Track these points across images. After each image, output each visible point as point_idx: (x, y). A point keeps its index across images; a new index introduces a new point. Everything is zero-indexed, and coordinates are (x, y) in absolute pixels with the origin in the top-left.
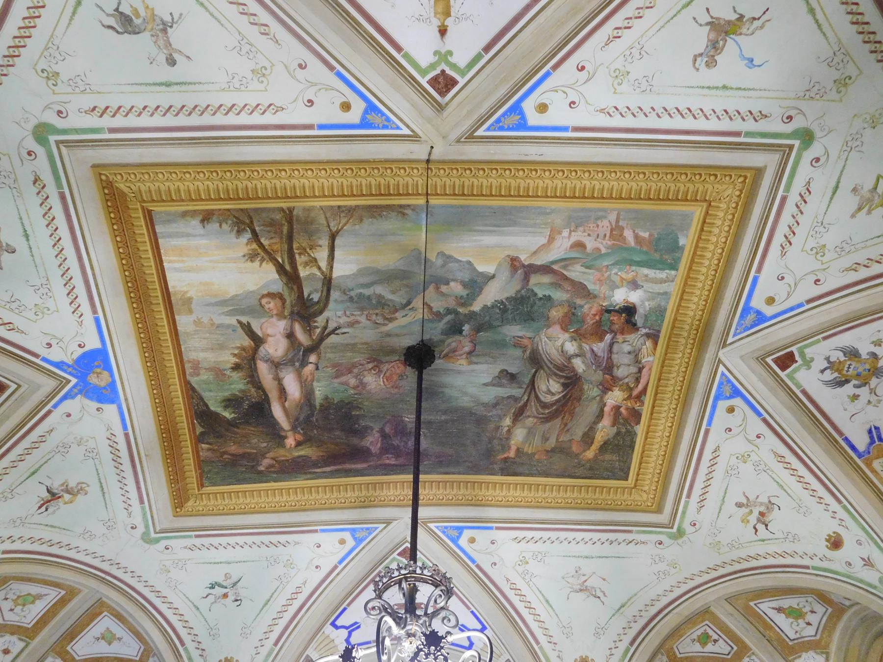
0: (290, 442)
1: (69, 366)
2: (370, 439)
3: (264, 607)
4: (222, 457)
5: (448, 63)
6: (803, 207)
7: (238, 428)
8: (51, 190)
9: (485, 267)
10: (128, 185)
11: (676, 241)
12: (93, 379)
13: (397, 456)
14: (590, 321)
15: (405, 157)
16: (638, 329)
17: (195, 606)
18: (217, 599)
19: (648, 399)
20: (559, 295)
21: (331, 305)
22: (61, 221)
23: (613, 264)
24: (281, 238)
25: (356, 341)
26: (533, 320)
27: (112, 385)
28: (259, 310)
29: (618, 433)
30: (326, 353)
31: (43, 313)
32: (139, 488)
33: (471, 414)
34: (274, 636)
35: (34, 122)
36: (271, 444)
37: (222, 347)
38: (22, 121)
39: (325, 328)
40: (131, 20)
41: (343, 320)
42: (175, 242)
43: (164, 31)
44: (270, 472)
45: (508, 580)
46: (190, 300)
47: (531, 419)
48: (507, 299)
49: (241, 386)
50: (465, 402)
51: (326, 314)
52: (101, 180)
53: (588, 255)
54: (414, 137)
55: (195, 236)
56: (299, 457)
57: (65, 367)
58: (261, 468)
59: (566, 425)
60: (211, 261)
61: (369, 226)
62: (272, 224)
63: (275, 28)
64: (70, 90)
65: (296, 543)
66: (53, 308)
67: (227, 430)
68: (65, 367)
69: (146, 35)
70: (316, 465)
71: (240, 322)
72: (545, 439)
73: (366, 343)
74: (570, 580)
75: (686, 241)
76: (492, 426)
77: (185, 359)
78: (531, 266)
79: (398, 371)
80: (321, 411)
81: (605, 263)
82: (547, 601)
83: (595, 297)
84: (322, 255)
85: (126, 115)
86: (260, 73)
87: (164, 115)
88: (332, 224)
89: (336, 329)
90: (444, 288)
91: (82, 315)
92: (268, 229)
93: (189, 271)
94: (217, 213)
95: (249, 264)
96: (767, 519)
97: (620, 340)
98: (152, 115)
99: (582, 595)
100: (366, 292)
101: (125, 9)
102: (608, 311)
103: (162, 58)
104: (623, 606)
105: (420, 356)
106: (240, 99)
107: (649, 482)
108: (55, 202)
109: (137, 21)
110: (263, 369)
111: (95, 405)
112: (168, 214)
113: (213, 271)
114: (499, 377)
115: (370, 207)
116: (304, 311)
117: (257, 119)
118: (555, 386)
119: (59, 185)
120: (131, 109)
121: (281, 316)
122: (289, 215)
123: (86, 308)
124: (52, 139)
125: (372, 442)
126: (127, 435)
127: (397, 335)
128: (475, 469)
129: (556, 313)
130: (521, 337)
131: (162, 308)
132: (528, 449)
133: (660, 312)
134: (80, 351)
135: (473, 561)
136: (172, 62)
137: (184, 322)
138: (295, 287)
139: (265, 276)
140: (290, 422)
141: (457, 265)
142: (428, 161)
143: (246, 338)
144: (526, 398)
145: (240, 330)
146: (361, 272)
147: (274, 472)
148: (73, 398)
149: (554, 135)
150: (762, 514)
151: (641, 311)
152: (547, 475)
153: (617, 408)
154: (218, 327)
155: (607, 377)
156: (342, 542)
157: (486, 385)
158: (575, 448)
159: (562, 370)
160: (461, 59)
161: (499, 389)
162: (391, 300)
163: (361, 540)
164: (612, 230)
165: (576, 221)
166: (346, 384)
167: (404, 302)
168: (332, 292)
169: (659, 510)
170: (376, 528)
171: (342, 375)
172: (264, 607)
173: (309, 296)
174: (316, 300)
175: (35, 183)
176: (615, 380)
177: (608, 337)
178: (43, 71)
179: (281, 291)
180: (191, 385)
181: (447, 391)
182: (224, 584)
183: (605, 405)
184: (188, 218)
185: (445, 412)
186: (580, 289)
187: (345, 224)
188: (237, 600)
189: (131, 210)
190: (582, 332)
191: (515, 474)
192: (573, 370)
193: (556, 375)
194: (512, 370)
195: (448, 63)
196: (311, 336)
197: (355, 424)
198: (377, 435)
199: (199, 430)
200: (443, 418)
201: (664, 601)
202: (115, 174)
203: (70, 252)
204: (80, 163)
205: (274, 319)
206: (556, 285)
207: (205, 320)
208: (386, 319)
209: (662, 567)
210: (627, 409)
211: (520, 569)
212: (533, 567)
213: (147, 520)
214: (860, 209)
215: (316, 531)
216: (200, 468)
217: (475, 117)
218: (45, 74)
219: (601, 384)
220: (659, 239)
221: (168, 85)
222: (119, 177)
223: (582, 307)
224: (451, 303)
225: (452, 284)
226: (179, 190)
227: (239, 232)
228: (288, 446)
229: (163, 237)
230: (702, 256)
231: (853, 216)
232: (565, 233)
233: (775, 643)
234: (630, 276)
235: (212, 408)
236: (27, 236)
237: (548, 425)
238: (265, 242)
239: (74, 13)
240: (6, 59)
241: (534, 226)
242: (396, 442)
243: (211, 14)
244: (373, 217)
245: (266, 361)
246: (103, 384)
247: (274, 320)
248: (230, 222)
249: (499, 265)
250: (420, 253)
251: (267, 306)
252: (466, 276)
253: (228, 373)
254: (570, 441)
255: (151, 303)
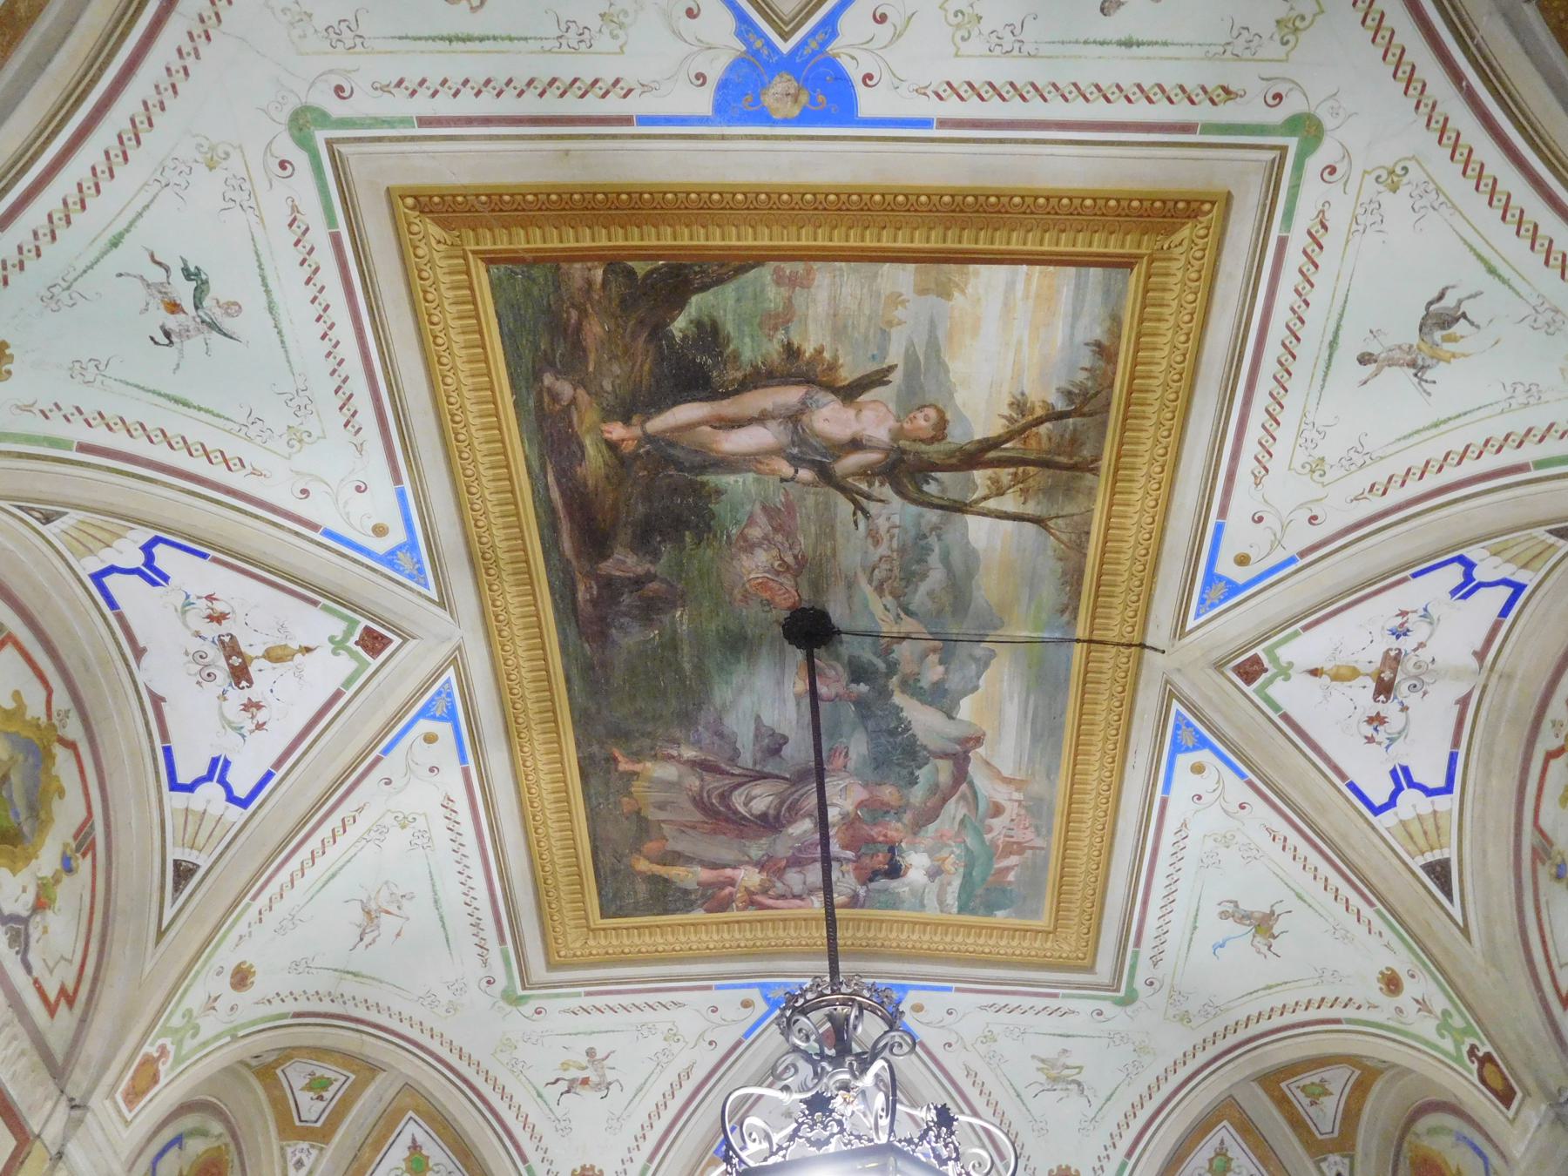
0: (617, 431)
1: (823, 45)
2: (631, 560)
3: (166, 396)
4: (573, 305)
5: (1275, 677)
6: (1146, 1094)
7: (647, 342)
8: (1203, 113)
9: (966, 709)
10: (1186, 243)
11: (1000, 908)
12: (781, 85)
13: (594, 602)
14: (874, 832)
15: (1152, 617)
16: (864, 884)
17: (121, 236)
18: (161, 290)
19: (752, 914)
20: (917, 795)
21: (913, 509)
22: (1141, 112)
23: (967, 849)
24: (1048, 452)
25: (840, 540)
26: (877, 768)
27: (765, 118)
28: (912, 399)
29: (686, 892)
30: (816, 494)
31: (958, 26)
32: (469, 121)
33: (699, 706)
34: (99, 437)
35: (1328, 122)
36: (611, 398)
37: (839, 330)
38: (1336, 105)
39: (869, 497)
40: (1443, 328)
41: (882, 524)
42: (1066, 293)
43: (1413, 364)
44: (540, 393)
45: (360, 810)
46: (944, 292)
47: (697, 783)
48: (914, 736)
49: (747, 354)
50: (722, 693)
51: (896, 501)
52: (1203, 202)
53: (982, 821)
54: (1180, 631)
55: (1073, 327)
56: (582, 447)
57: (820, 37)
58: (548, 379)
59: (694, 828)
60: (1020, 342)
61: (1050, 568)
62: (1075, 442)
63: (1377, 504)
64: (1364, 198)
65: (359, 448)
66: (965, 48)
67: (641, 322)
68: (820, 37)
69: (1415, 339)
70: (563, 475)
71: (891, 369)
72: (661, 806)
73: (834, 555)
74: (385, 893)
75: (1001, 917)
76: (678, 734)
77: (816, 265)
78: (967, 759)
79: (777, 599)
80: (692, 483)
81: (968, 841)
82: (333, 876)
83: (915, 834)
84: (1009, 503)
85: (1301, 271)
86: (1317, 467)
87: (1288, 327)
88: (1060, 521)
89: (866, 513)
90: (933, 658)
91: (941, 98)
92: (1067, 436)
93: (1005, 304)
94: (1110, 368)
95: (1007, 400)
96: (579, 1089)
97: (844, 868)
98: (1292, 310)
99: (359, 916)
100: (934, 559)
101: (1460, 328)
102: (892, 850)
103: (1374, 348)
104: (355, 975)
105: (810, 630)
106: (1285, 434)
107: (597, 945)
108: (1181, 112)
109: (1438, 335)
110: (791, 396)
111: (715, 73)
112: (1122, 295)
113: (1002, 342)
114: (773, 734)
115: (1080, 572)
116: (904, 469)
117: (1250, 447)
118: (759, 806)
119: (1210, 128)
120: (1309, 281)
121: (897, 434)
122: (1090, 466)
123: (953, 108)
124: (1293, 143)
125: (624, 562)
126: (626, 120)
127: (850, 597)
128: (583, 720)
129: (888, 793)
130: (847, 755)
131: (932, 245)
132: (637, 787)
133: (894, 903)
134: (856, 75)
135: (386, 751)
136: (1364, 359)
137: (902, 277)
138: (954, 461)
139: (979, 412)
140: (664, 431)
141: (973, 673)
142: (1142, 646)
143: (857, 375)
144: (737, 771)
145: (872, 367)
146: (971, 555)
147: (540, 401)
148: (739, 34)
149: (1160, 777)
150: (585, 1081)
151: (894, 884)
152: (593, 817)
153: (732, 882)
154: (883, 332)
155: (784, 863)
156: (380, 531)
157: (758, 718)
158: (651, 846)
159: (789, 809)
160: (1278, 690)
161: (751, 735)
162: (916, 590)
163: (391, 564)
164: (1019, 843)
165: (1035, 809)
166: (751, 521)
167: (912, 607)
168: (940, 512)
169: (551, 966)
170: (426, 586)
171: (770, 518)
172: (166, 396)
173: (936, 479)
174: (926, 488)
175: (1226, 90)
176: (780, 873)
177: (850, 854)
178: (1405, 169)
179: (949, 439)
180: (753, 267)
181: (743, 666)
182: (207, 302)
183: (735, 868)
184: (1108, 324)
185: (699, 668)
186: (931, 815)
187: (1058, 539)
188: (167, 334)
189: (1141, 233)
190: (857, 824)
191: (584, 776)
192: (791, 822)
193: (782, 803)
194: (787, 751)
195: (1275, 677)
196: (853, 474)
197: (661, 533)
198: (640, 570)
199: (641, 268)
200: (687, 666)
201: (382, 1020)
202: (1208, 228)
203: (1077, 111)
204: (1239, 174)
205: (892, 423)
206: (934, 788)
207: (900, 313)
208: (881, 584)
209: (445, 996)
210: (731, 894)
211: (388, 820)
212: (397, 839)
213: (370, 127)
214: (1043, 1061)
215: (397, 479)
216: (537, 261)
217: (1200, 703)
218: (1399, 171)
219: (770, 858)
220: (1004, 891)
221: (1333, 344)
222: (1202, 232)
223: (899, 820)
224: (906, 668)
225: (941, 669)
226: (1159, 320)
227: (1068, 395)
228: (605, 427)
229: (1078, 276)
230: (980, 936)
231: (1033, 1057)
232: (1016, 796)
233: (355, 1166)
234: (948, 866)
235: (694, 299)
236: (1128, 44)
237: (689, 805)
238: (1044, 429)
239: (1480, 257)
240: (1442, 120)
241: (1031, 760)
242: (626, 599)
243: (1417, 432)
244: (1064, 573)
245: (803, 402)
246: (768, 100)
247: (891, 423)
248: (1090, 384)
249: (970, 724)
250: (996, 628)
251: (920, 415)
252: (954, 682)
253: (780, 335)
254: (664, 838)
255: (947, 228)
